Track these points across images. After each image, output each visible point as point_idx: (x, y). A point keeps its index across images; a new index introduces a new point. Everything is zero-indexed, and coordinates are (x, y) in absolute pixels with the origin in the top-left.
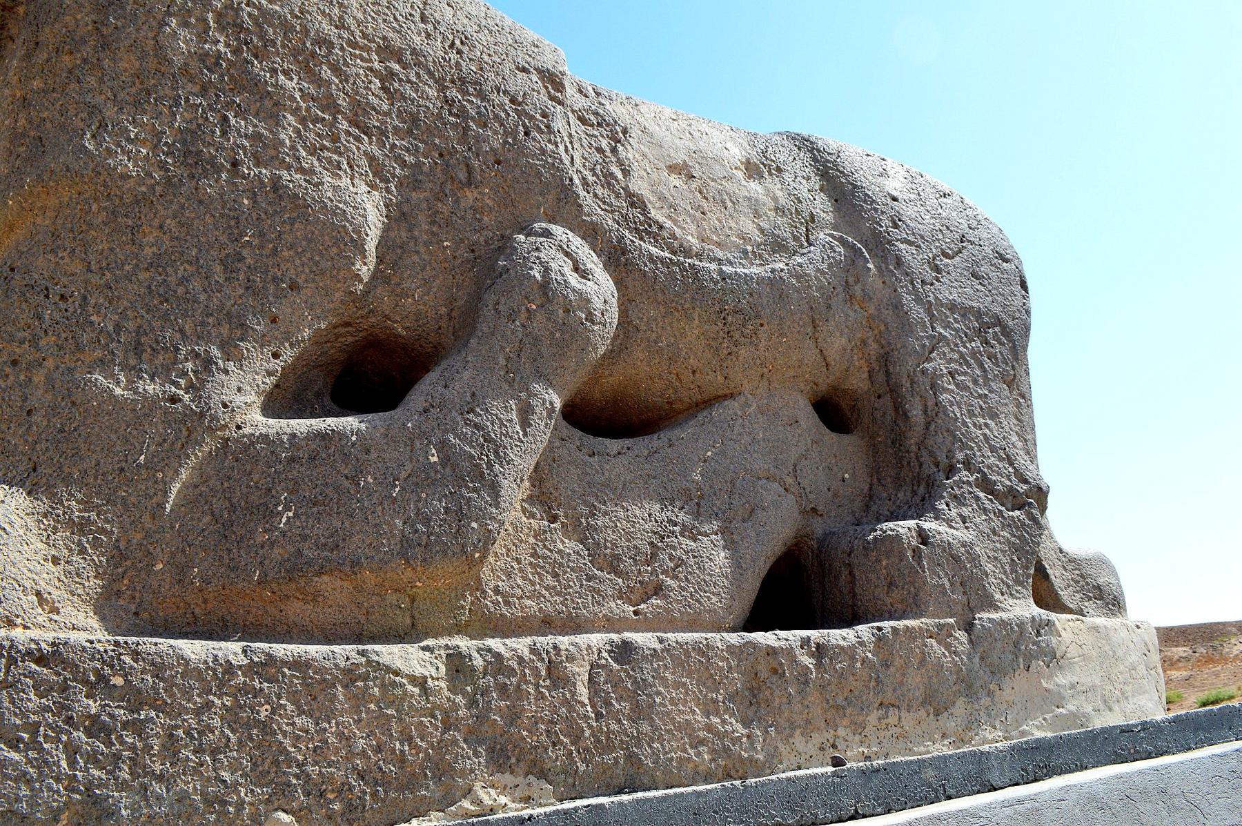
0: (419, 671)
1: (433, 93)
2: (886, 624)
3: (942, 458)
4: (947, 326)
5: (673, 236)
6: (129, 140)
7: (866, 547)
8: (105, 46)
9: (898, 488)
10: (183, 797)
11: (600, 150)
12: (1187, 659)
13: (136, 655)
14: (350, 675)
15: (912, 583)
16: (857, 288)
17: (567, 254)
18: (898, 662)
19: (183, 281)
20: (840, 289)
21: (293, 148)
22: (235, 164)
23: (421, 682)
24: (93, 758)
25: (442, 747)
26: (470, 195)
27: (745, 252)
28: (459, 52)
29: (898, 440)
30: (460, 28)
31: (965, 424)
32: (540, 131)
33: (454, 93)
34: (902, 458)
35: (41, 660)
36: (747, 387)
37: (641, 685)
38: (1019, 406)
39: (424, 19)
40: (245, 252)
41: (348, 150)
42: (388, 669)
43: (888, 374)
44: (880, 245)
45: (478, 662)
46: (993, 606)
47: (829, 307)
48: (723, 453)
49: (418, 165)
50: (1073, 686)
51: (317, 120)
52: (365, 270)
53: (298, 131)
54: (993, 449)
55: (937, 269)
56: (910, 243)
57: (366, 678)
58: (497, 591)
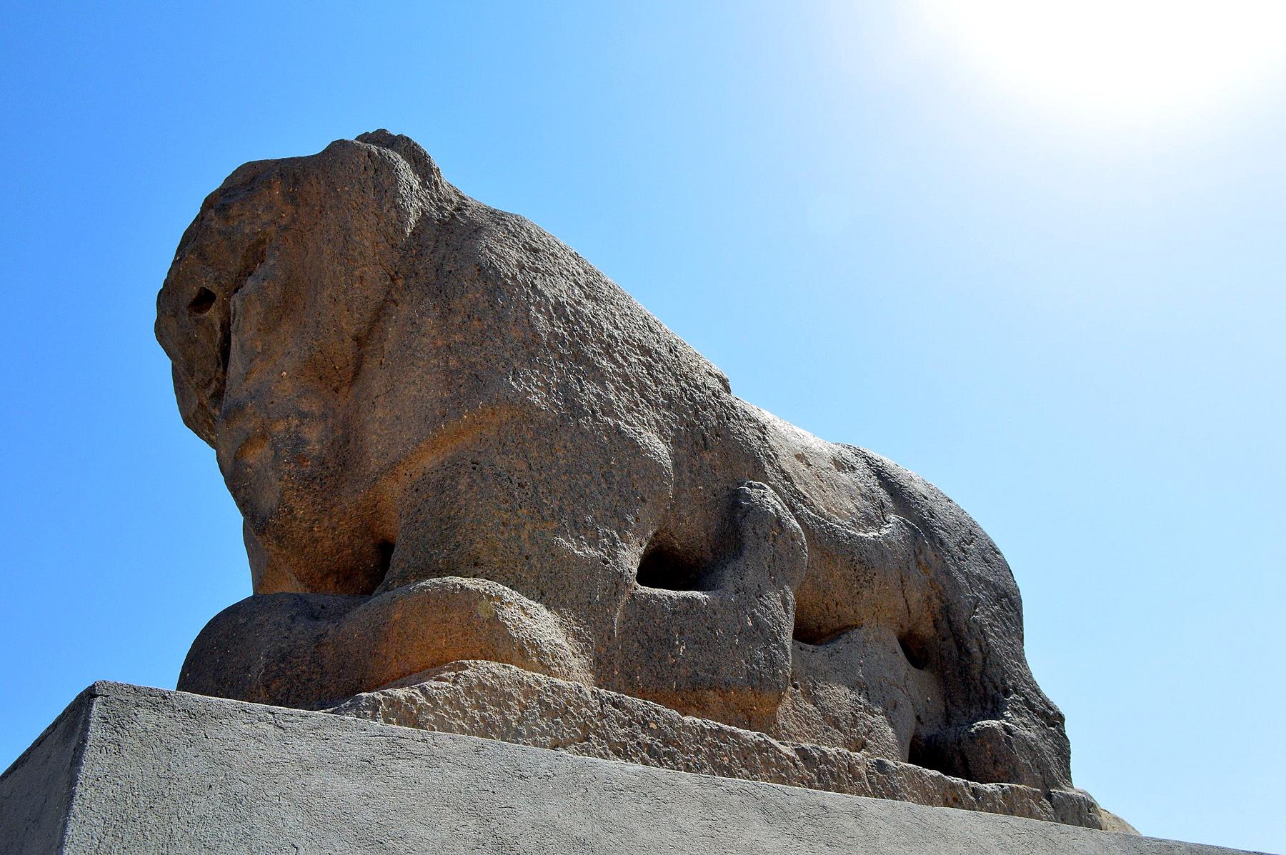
3: (998, 683)
7: (972, 737)
15: (1010, 760)
16: (922, 557)
26: (707, 456)
29: (964, 671)
34: (969, 684)
36: (865, 621)
40: (614, 472)
43: (950, 622)
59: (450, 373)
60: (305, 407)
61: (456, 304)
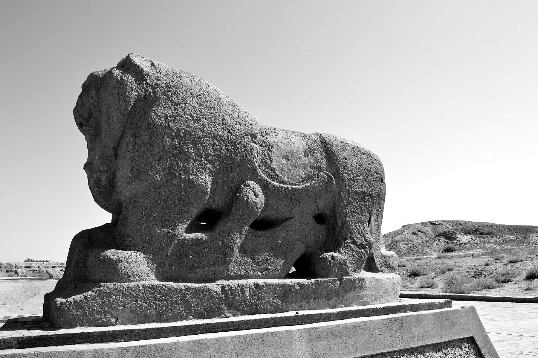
0: (216, 290)
1: (224, 148)
2: (319, 279)
3: (344, 236)
4: (353, 198)
5: (281, 179)
6: (158, 171)
8: (151, 145)
9: (332, 241)
10: (174, 313)
11: (265, 155)
12: (513, 241)
13: (165, 287)
14: (203, 291)
17: (253, 191)
18: (320, 288)
19: (170, 204)
20: (324, 189)
21: (192, 169)
22: (180, 175)
23: (216, 292)
24: (159, 306)
25: (220, 305)
26: (232, 174)
27: (300, 181)
28: (231, 133)
29: (334, 229)
30: (231, 125)
31: (352, 226)
32: (250, 155)
33: (229, 147)
35: (150, 288)
37: (260, 293)
38: (378, 211)
39: (223, 125)
41: (204, 167)
42: (210, 290)
44: (338, 175)
45: (227, 288)
46: (348, 275)
47: (320, 195)
48: (287, 234)
49: (220, 168)
50: (366, 295)
51: (198, 160)
52: (207, 198)
53: (193, 164)
54: (359, 233)
55: (354, 181)
56: (347, 173)
57: (206, 291)
58: (232, 270)
59: (133, 168)
60: (102, 169)
61: (138, 141)
